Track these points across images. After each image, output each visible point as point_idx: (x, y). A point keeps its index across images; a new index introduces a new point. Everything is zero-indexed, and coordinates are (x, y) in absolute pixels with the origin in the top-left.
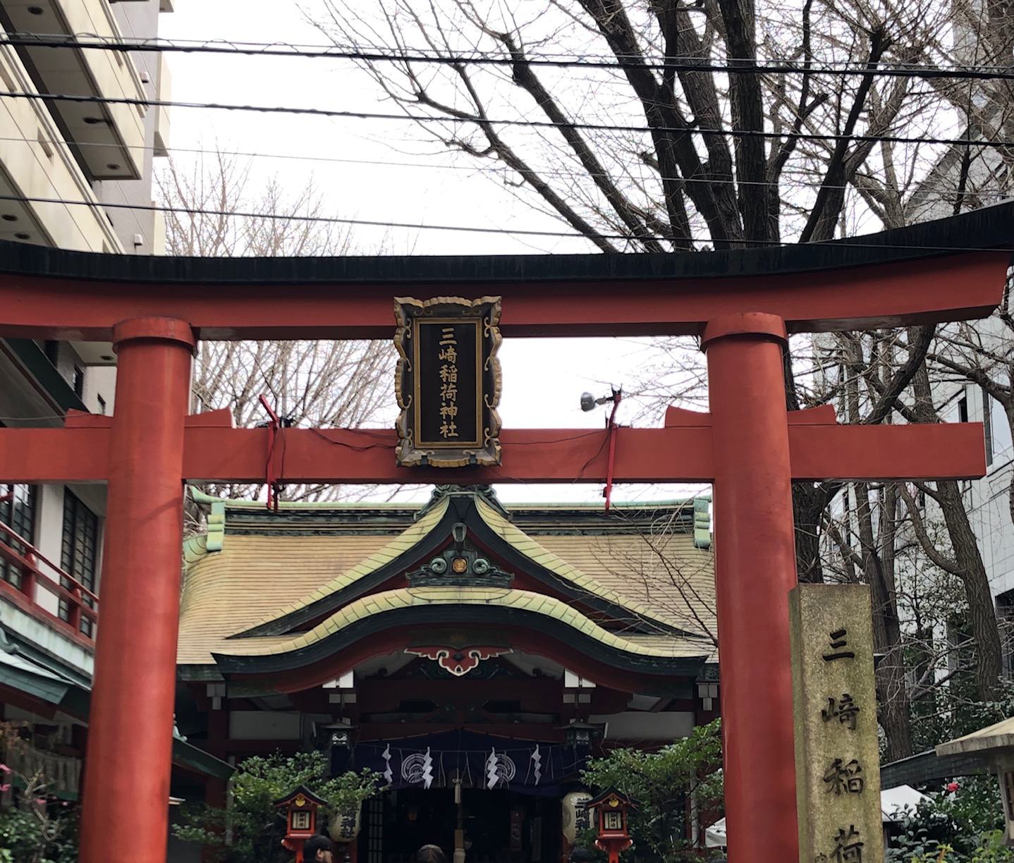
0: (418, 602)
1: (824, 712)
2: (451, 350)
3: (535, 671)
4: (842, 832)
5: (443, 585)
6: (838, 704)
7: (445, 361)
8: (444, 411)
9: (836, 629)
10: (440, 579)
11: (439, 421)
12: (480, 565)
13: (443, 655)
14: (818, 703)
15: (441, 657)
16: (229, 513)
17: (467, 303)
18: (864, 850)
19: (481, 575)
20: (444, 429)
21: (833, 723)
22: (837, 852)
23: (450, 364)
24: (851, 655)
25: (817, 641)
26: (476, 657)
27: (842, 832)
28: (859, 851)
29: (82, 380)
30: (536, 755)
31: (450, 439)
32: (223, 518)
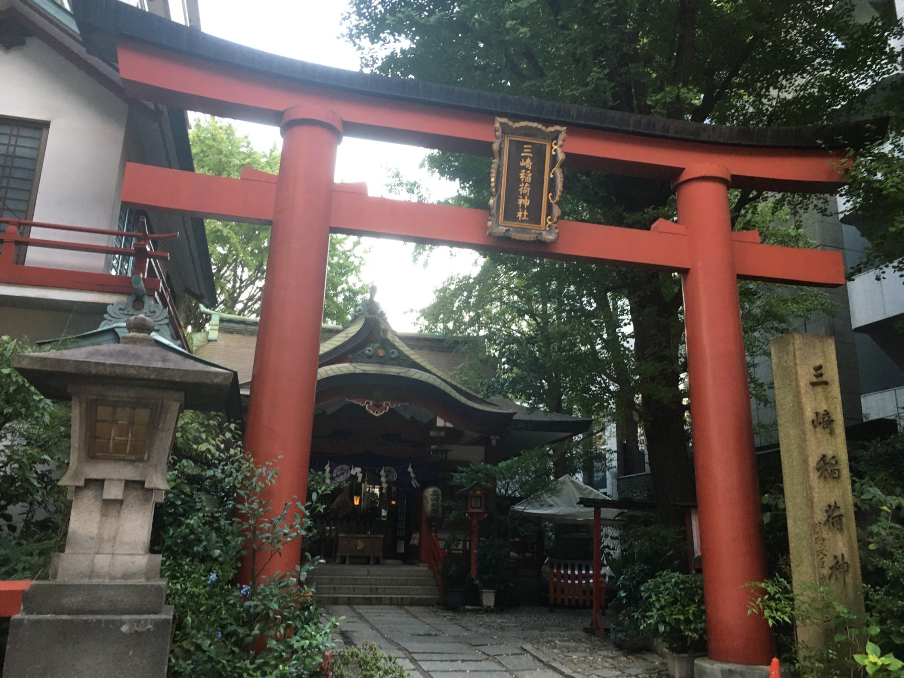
0: (357, 371)
1: (813, 421)
2: (528, 160)
3: (412, 418)
4: (830, 506)
5: (371, 363)
6: (820, 416)
7: (524, 167)
8: (520, 202)
9: (818, 364)
10: (369, 359)
11: (517, 208)
12: (393, 353)
13: (368, 403)
14: (809, 415)
15: (367, 405)
16: (222, 320)
17: (544, 128)
18: (844, 520)
19: (394, 359)
20: (520, 214)
21: (819, 429)
22: (827, 521)
23: (527, 169)
24: (826, 383)
25: (805, 375)
26: (387, 406)
27: (830, 506)
28: (840, 519)
29: (312, 125)
30: (410, 470)
31: (522, 221)
32: (218, 323)
